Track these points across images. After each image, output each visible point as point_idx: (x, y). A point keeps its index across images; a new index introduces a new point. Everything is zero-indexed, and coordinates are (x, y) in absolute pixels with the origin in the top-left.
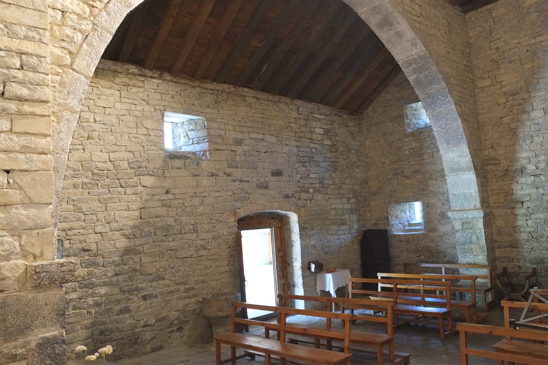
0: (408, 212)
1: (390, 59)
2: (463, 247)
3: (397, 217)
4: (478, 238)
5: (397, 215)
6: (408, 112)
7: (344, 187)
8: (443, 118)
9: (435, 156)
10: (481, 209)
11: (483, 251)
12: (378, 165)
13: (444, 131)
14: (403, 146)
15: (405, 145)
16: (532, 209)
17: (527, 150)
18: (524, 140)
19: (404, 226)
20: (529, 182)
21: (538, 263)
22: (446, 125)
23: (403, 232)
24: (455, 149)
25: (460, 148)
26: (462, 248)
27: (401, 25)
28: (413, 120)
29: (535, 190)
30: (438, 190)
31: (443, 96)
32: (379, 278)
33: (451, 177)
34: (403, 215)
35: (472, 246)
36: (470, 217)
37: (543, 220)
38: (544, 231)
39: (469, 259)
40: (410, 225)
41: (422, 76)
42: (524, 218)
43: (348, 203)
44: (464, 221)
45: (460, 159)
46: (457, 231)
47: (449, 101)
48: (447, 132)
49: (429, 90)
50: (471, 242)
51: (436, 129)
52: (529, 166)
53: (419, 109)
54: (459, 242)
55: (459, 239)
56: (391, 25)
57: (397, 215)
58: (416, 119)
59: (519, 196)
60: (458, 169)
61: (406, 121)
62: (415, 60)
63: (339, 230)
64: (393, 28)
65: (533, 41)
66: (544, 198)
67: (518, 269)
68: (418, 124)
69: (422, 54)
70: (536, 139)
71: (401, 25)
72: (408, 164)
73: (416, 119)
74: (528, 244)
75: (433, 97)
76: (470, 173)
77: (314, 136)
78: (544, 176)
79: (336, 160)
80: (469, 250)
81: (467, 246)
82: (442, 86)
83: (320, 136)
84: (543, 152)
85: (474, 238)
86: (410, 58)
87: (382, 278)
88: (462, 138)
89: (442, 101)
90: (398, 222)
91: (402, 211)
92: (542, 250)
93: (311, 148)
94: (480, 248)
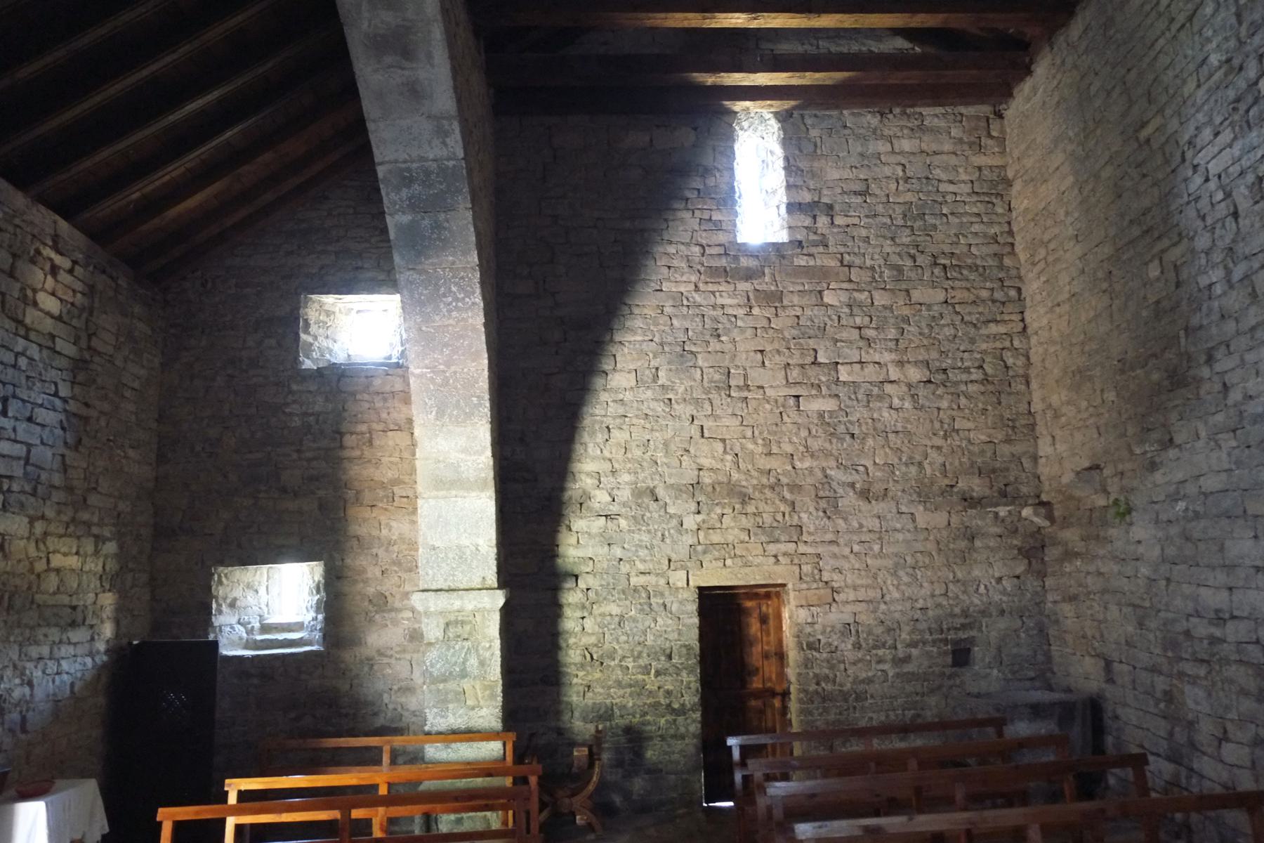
0: (262, 590)
1: (365, 150)
2: (441, 686)
3: (232, 605)
4: (482, 663)
5: (235, 600)
6: (312, 313)
7: (93, 499)
8: (446, 345)
9: (377, 443)
10: (500, 587)
11: (492, 696)
12: (198, 448)
13: (439, 380)
14: (287, 405)
15: (294, 402)
16: (597, 593)
17: (593, 459)
18: (593, 434)
19: (250, 631)
20: (594, 531)
21: (601, 718)
22: (448, 365)
23: (246, 647)
24: (458, 430)
25: (469, 429)
26: (439, 691)
27: (432, 66)
28: (320, 339)
29: (606, 548)
30: (375, 533)
31: (461, 289)
32: (232, 799)
33: (432, 502)
34: (250, 599)
35: (466, 684)
36: (470, 607)
37: (617, 619)
38: (618, 642)
39: (456, 719)
40: (265, 628)
41: (426, 222)
42: (579, 614)
43: (97, 552)
44: (452, 618)
45: (463, 456)
46: (430, 644)
47: (474, 304)
48: (446, 383)
49: (432, 264)
50: (464, 674)
51: (418, 371)
52: (597, 492)
53: (337, 314)
54: (431, 673)
55: (432, 666)
56: (407, 53)
57: (235, 600)
58: (327, 337)
59: (571, 560)
60: (452, 483)
61: (303, 336)
62: (427, 173)
63: (61, 642)
64: (407, 64)
65: (628, 224)
66: (622, 567)
67: (555, 736)
68: (330, 351)
69: (451, 163)
70: (616, 433)
71: (432, 66)
72: (295, 456)
73: (327, 337)
74: (581, 674)
75: (436, 284)
76: (483, 495)
77: (31, 316)
78: (626, 518)
79: (84, 411)
80: (457, 693)
81: (452, 685)
82: (468, 262)
83: (49, 321)
84: (629, 465)
85: (473, 661)
86: (415, 165)
87: (243, 796)
88: (480, 405)
89: (457, 300)
90: (234, 620)
91: (249, 586)
92: (609, 688)
93: (17, 355)
94: (485, 688)
